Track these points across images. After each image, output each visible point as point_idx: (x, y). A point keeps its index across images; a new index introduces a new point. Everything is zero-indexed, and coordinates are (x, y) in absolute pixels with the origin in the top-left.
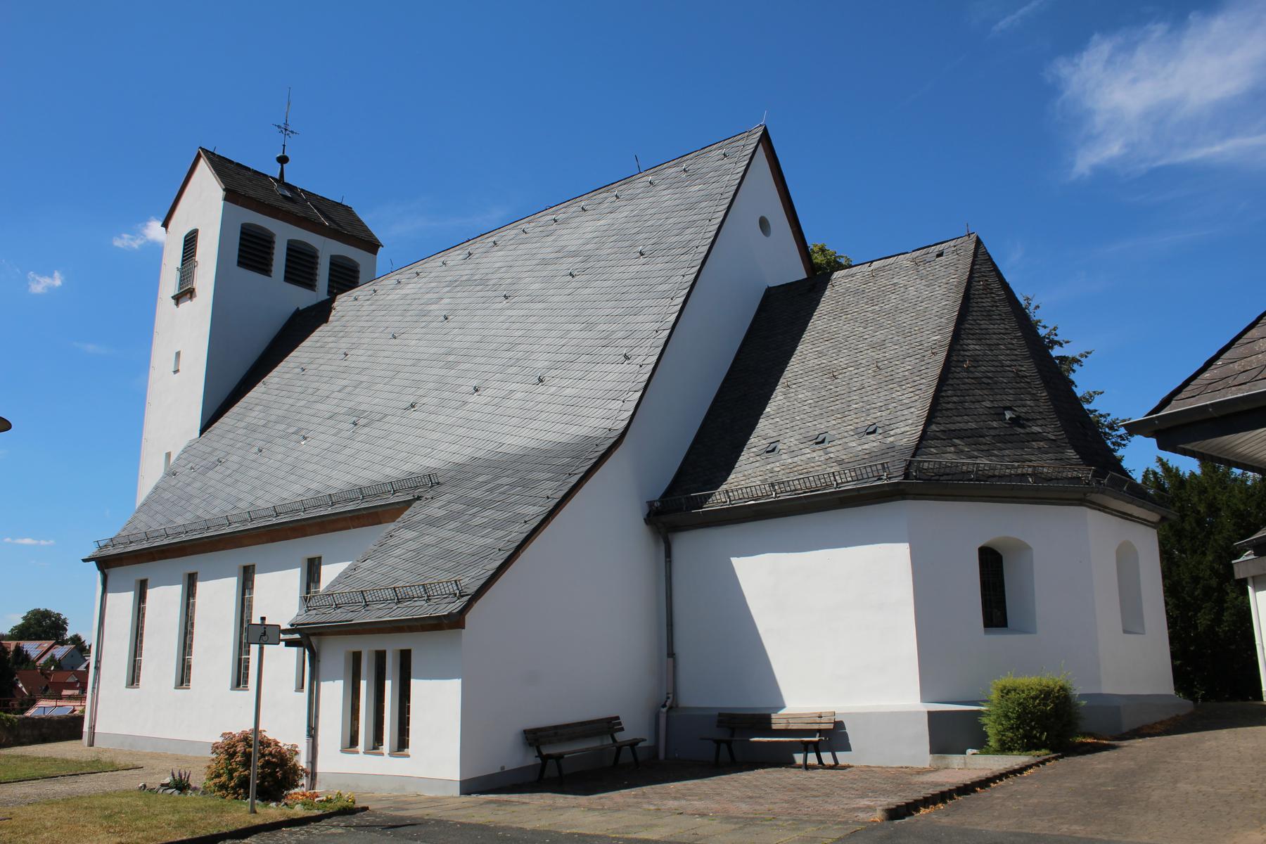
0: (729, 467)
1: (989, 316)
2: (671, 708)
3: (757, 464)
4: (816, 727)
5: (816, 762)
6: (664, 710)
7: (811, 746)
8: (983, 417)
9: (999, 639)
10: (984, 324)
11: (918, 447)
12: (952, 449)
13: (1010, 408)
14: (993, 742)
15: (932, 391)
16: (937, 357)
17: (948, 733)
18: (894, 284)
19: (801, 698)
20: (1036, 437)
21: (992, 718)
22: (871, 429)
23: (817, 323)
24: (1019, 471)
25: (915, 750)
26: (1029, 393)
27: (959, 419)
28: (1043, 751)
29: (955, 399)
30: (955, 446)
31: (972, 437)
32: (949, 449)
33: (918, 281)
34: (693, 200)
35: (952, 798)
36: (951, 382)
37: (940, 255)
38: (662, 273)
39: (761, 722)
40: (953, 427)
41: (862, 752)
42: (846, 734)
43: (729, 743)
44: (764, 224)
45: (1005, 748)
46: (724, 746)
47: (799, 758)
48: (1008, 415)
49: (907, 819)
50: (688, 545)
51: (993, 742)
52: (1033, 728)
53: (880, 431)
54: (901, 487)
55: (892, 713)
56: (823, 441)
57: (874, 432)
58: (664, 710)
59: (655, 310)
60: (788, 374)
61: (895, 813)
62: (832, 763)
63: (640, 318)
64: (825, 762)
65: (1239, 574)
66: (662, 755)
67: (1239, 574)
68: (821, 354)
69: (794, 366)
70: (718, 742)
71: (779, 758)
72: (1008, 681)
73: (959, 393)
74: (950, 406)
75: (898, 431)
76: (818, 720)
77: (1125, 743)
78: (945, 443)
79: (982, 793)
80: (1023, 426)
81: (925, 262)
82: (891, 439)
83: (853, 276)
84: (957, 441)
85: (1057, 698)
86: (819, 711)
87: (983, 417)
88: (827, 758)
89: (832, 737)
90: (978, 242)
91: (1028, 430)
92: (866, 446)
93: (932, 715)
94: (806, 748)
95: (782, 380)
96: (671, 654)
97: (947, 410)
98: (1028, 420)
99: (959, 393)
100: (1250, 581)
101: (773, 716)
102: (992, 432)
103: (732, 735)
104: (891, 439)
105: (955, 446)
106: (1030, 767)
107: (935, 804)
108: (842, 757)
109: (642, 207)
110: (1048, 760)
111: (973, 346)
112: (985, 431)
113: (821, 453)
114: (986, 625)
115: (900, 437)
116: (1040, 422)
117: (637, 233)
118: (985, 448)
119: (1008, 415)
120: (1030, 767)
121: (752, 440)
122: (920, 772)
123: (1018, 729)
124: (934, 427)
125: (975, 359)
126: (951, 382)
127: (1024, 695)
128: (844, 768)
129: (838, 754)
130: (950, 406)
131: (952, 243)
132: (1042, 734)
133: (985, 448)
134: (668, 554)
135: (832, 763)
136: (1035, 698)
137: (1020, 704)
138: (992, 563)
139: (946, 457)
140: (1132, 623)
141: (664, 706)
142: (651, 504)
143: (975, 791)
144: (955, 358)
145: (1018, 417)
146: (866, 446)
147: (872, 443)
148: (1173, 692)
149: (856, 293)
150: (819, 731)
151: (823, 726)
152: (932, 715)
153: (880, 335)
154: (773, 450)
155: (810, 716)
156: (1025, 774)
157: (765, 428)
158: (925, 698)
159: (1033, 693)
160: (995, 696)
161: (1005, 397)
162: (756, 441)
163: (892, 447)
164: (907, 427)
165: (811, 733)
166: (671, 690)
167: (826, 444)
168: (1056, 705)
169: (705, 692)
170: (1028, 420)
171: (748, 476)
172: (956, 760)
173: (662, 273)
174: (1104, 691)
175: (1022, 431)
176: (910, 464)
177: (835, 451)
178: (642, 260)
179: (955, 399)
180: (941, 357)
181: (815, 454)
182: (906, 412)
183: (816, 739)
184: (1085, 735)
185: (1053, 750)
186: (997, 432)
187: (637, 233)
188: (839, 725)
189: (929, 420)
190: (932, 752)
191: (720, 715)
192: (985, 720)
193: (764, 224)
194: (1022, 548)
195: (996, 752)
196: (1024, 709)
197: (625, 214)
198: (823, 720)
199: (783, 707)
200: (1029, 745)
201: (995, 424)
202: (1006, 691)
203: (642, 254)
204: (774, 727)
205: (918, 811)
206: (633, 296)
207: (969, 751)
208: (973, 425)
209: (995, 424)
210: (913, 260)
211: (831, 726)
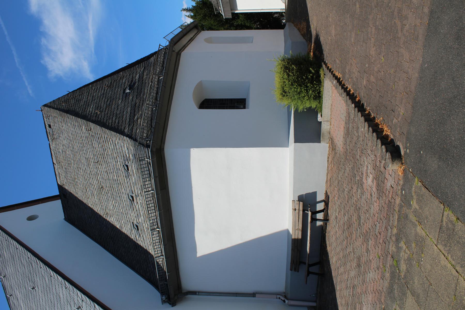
0: (146, 252)
1: (79, 101)
2: (285, 297)
3: (144, 236)
4: (301, 213)
5: (322, 214)
6: (287, 301)
7: (313, 217)
8: (126, 104)
9: (251, 103)
10: (82, 103)
11: (135, 140)
12: (139, 120)
13: (125, 90)
14: (314, 105)
15: (107, 131)
16: (92, 128)
17: (308, 129)
18: (62, 151)
19: (283, 219)
20: (141, 77)
21: (300, 102)
22: (126, 168)
23: (80, 195)
24: (156, 83)
25: (319, 152)
26: (119, 81)
27: (124, 117)
28: (321, 72)
29: (114, 119)
30: (138, 119)
31: (135, 109)
32: (139, 122)
33: (61, 138)
34: (10, 256)
35: (369, 114)
36: (105, 121)
37: (50, 126)
38: (41, 279)
39: (297, 245)
40: (128, 120)
41: (318, 186)
42: (306, 194)
43: (310, 266)
44: (31, 218)
45: (318, 97)
46: (311, 269)
47: (319, 223)
48: (128, 91)
49: (398, 143)
50: (190, 279)
51: (314, 105)
52: (307, 78)
53: (127, 163)
54: (154, 150)
55: (294, 165)
56: (132, 197)
57: (127, 166)
58: (287, 301)
59: (57, 287)
60: (101, 213)
61: (395, 153)
62: (323, 203)
63: (61, 296)
64: (322, 208)
65: (230, 16)
66: (314, 304)
67: (230, 16)
68: (93, 194)
69: (98, 209)
70: (309, 273)
71: (320, 236)
72: (277, 93)
73: (111, 116)
74: (117, 122)
75: (127, 151)
76: (297, 211)
77: (314, 33)
78: (135, 124)
79: (362, 95)
80: (135, 84)
81: (53, 135)
82: (131, 156)
83: (59, 174)
84: (136, 117)
85: (288, 63)
86: (291, 210)
87: (126, 104)
88: (320, 207)
89: (306, 203)
90: (45, 105)
91: (137, 81)
92: (134, 171)
93: (297, 140)
94: (314, 220)
95: (104, 217)
96: (253, 295)
97: (118, 123)
98: (132, 81)
99: (111, 116)
100: (233, 11)
101: (293, 237)
102: (135, 99)
103: (305, 263)
104: (131, 156)
105: (138, 119)
106: (334, 75)
107: (377, 125)
108: (320, 197)
109: (15, 284)
110: (328, 68)
111: (91, 109)
112: (133, 103)
113: (138, 198)
114: (244, 108)
115: (130, 150)
116: (134, 75)
117: (25, 288)
118: (141, 102)
119: (128, 91)
120: (334, 75)
121: (133, 237)
122: (333, 147)
123: (307, 87)
124: (126, 131)
125: (97, 108)
126: (105, 121)
127: (287, 82)
128: (327, 196)
129: (317, 201)
130: (117, 122)
131: (45, 119)
132: (310, 72)
133: (141, 102)
134: (194, 293)
135: (323, 203)
136: (288, 75)
137: (292, 85)
138: (207, 104)
139: (142, 123)
140: (249, 40)
141: (284, 301)
142: (163, 302)
143: (359, 101)
144: (94, 118)
145: (130, 86)
146: (134, 171)
147: (133, 167)
148: (283, 30)
149: (66, 172)
150: (304, 211)
151: (301, 208)
152: (297, 140)
153: (84, 161)
154: (137, 226)
155: (294, 216)
156: (339, 75)
157: (127, 230)
158: (286, 145)
159: (286, 76)
160: (286, 102)
161: (118, 93)
162: (133, 235)
163: (134, 155)
164: (124, 146)
165: (305, 216)
166: (275, 296)
167: (134, 195)
168: (293, 64)
169: (277, 274)
170: (132, 81)
171: (149, 241)
172: (325, 127)
173: (41, 279)
174: (284, 51)
175: (137, 83)
176: (140, 143)
177: (137, 190)
178: (36, 288)
179: (114, 119)
180: (92, 125)
181: (139, 202)
182: (118, 147)
183: (310, 213)
184: (309, 53)
185: (320, 66)
186: (135, 96)
187: (25, 288)
188: (301, 198)
189: (122, 133)
190: (319, 142)
191: (291, 270)
192: (301, 108)
193: (31, 218)
194: (200, 87)
195: (320, 103)
196: (295, 82)
197: (18, 293)
198: (297, 208)
199: (288, 231)
200: (317, 81)
201: (131, 98)
202: (284, 93)
203: (33, 288)
204: (300, 237)
205: (387, 136)
206: (52, 297)
207: (319, 119)
208: (129, 109)
209: (131, 98)
210: (52, 141)
211: (301, 203)
